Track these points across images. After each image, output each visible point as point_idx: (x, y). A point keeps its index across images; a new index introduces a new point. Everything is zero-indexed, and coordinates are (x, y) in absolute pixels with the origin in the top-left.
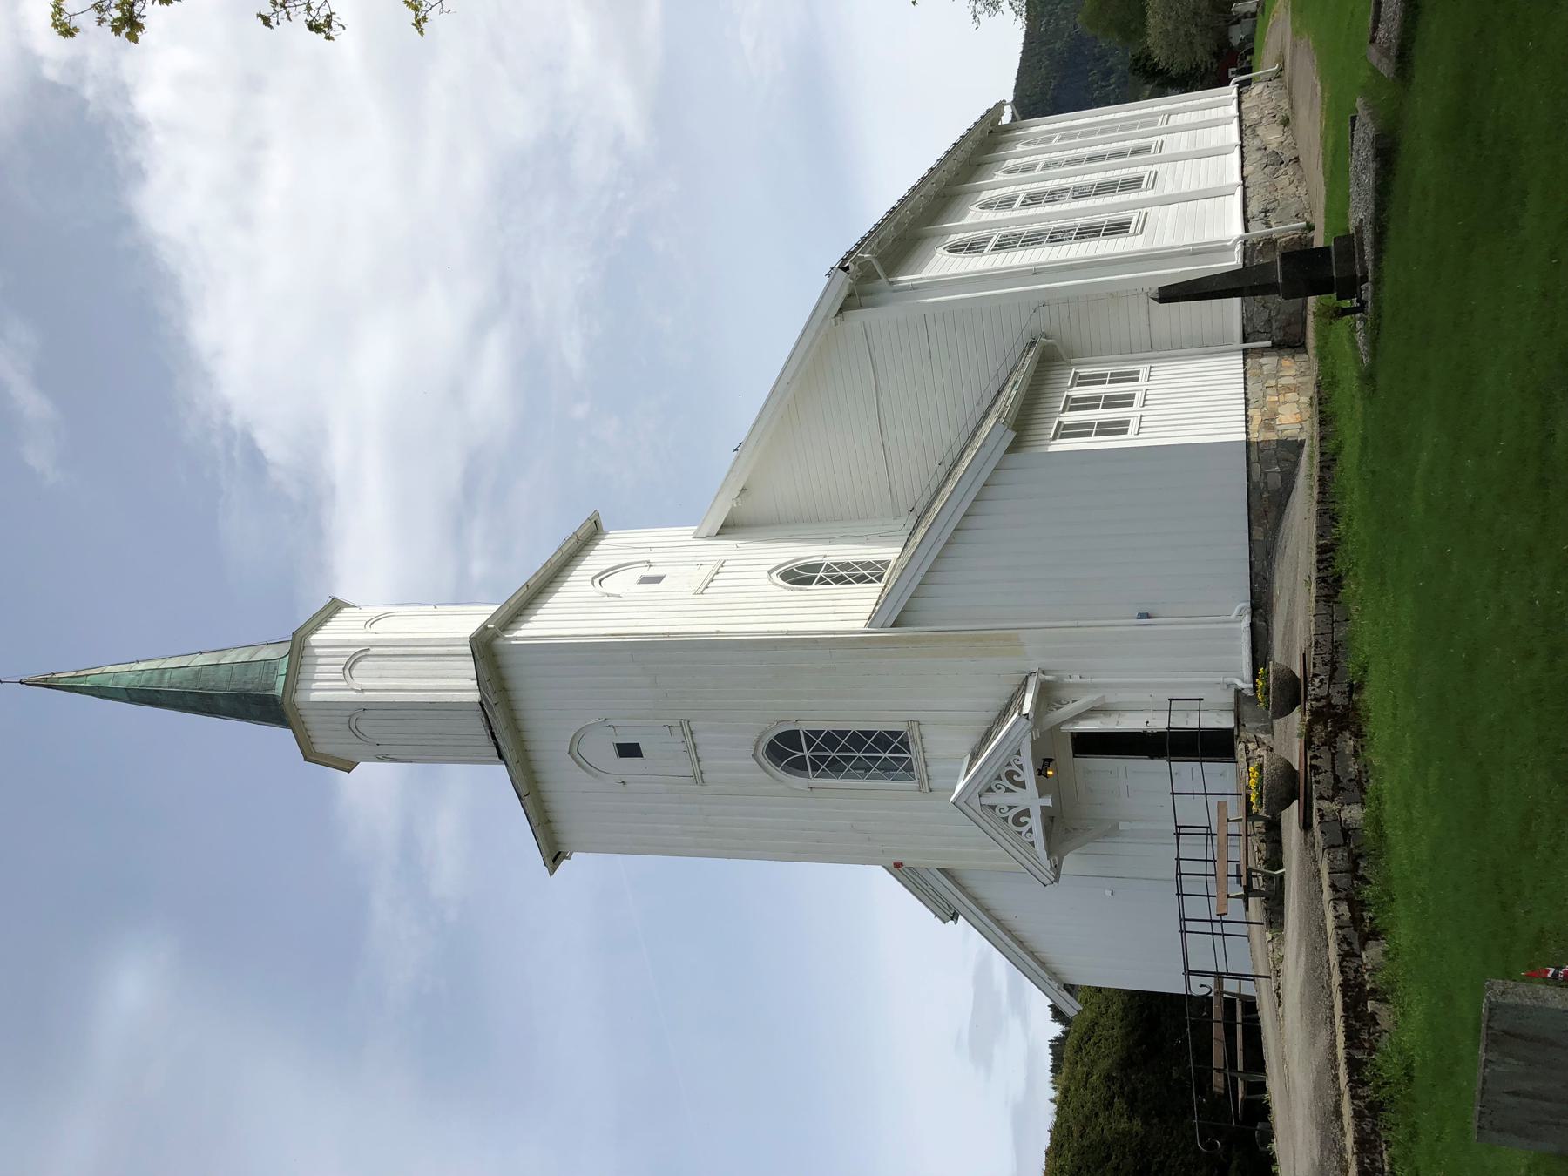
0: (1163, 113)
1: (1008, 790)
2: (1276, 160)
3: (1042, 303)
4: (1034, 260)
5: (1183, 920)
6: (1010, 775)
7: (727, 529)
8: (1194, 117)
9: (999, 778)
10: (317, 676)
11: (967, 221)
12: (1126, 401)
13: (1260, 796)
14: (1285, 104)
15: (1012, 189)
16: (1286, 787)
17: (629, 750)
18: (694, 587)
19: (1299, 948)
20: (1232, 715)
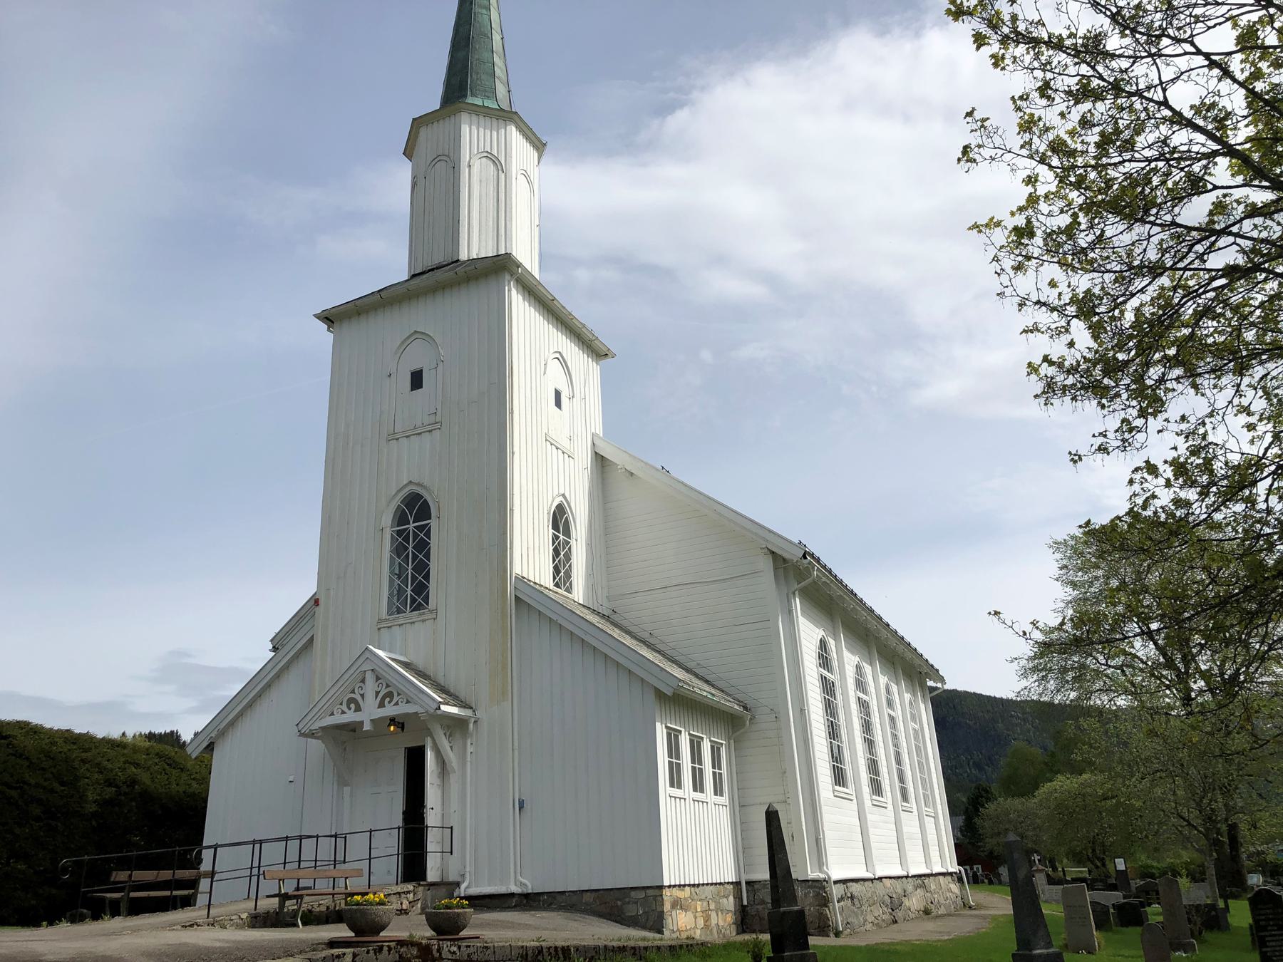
0: (936, 813)
1: (377, 693)
2: (895, 904)
3: (778, 715)
4: (812, 708)
5: (261, 842)
6: (390, 695)
7: (600, 461)
8: (932, 838)
9: (388, 686)
10: (482, 130)
11: (846, 654)
12: (698, 785)
13: (358, 904)
14: (942, 911)
15: (873, 690)
16: (365, 925)
17: (417, 380)
18: (553, 434)
19: (227, 942)
20: (438, 880)
